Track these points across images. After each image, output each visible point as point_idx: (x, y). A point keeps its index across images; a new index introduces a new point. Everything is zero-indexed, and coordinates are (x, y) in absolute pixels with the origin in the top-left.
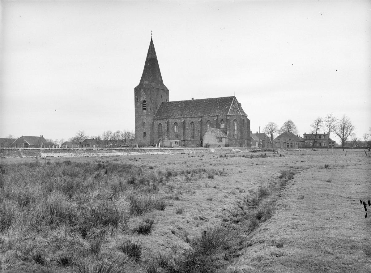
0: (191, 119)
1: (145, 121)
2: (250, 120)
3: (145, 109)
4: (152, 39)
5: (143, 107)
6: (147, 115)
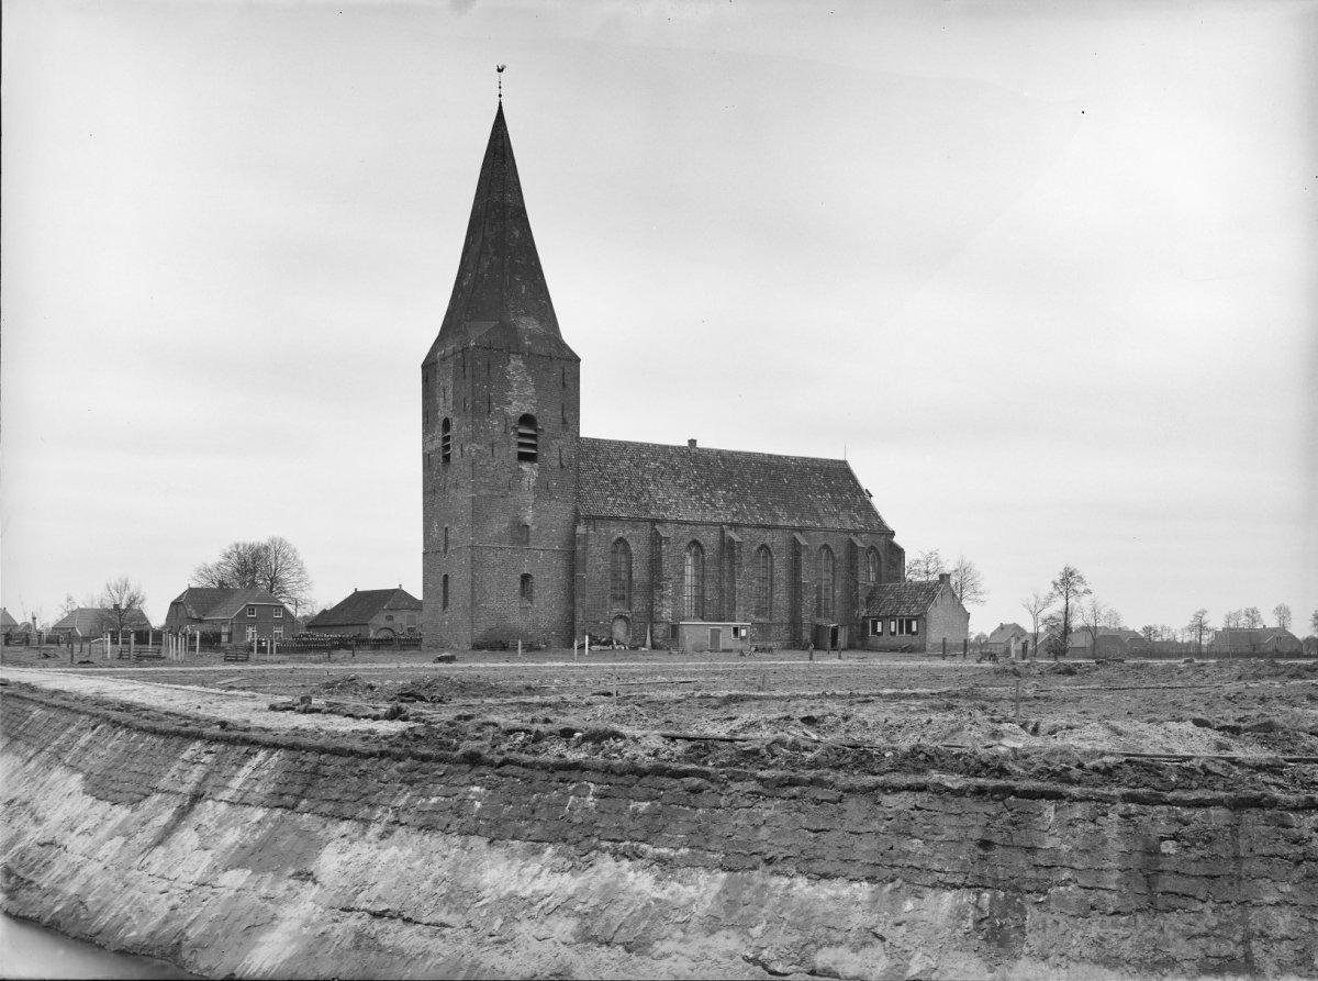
0: (759, 532)
1: (528, 517)
4: (500, 107)
5: (521, 445)
6: (543, 490)
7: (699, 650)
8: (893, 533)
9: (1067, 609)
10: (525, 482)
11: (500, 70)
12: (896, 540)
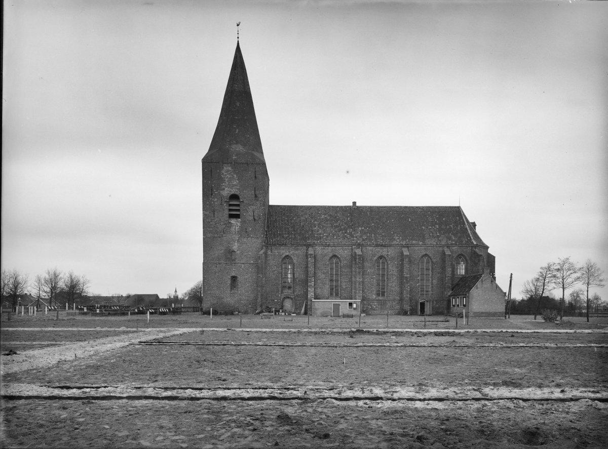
0: (378, 249)
1: (235, 247)
2: (494, 257)
3: (237, 216)
5: (230, 210)
6: (244, 232)
7: (324, 315)
8: (488, 247)
9: (564, 290)
10: (233, 229)
11: (238, 25)
12: (490, 251)
